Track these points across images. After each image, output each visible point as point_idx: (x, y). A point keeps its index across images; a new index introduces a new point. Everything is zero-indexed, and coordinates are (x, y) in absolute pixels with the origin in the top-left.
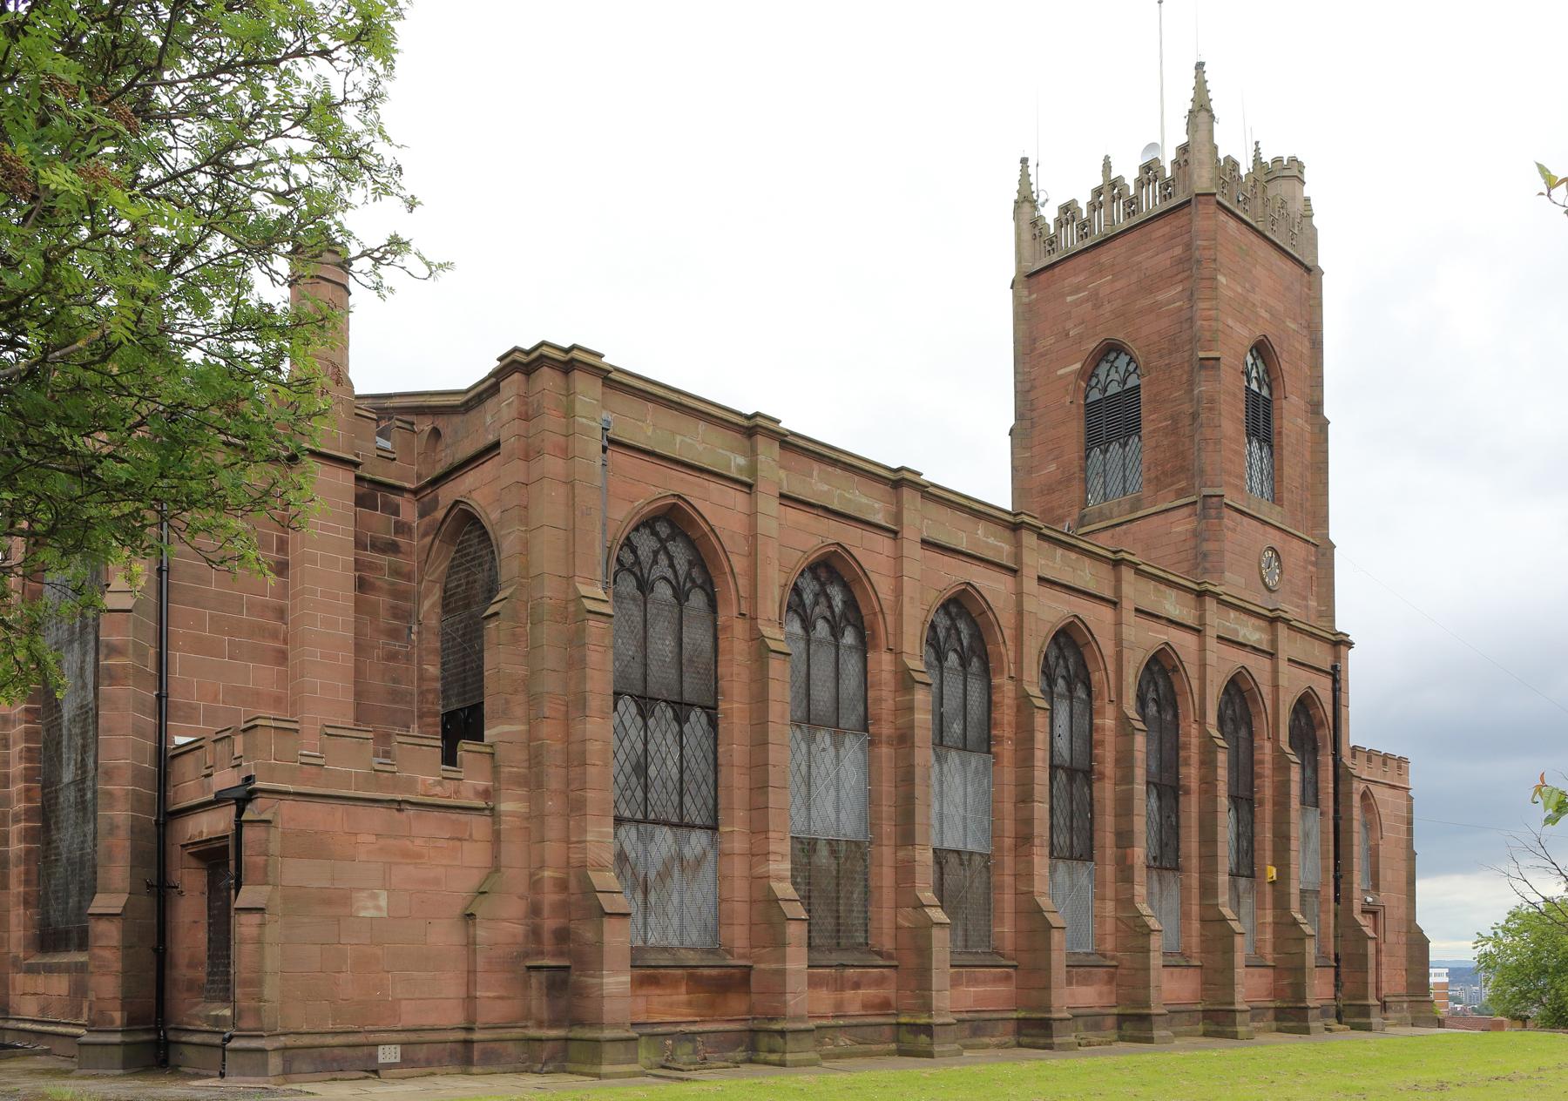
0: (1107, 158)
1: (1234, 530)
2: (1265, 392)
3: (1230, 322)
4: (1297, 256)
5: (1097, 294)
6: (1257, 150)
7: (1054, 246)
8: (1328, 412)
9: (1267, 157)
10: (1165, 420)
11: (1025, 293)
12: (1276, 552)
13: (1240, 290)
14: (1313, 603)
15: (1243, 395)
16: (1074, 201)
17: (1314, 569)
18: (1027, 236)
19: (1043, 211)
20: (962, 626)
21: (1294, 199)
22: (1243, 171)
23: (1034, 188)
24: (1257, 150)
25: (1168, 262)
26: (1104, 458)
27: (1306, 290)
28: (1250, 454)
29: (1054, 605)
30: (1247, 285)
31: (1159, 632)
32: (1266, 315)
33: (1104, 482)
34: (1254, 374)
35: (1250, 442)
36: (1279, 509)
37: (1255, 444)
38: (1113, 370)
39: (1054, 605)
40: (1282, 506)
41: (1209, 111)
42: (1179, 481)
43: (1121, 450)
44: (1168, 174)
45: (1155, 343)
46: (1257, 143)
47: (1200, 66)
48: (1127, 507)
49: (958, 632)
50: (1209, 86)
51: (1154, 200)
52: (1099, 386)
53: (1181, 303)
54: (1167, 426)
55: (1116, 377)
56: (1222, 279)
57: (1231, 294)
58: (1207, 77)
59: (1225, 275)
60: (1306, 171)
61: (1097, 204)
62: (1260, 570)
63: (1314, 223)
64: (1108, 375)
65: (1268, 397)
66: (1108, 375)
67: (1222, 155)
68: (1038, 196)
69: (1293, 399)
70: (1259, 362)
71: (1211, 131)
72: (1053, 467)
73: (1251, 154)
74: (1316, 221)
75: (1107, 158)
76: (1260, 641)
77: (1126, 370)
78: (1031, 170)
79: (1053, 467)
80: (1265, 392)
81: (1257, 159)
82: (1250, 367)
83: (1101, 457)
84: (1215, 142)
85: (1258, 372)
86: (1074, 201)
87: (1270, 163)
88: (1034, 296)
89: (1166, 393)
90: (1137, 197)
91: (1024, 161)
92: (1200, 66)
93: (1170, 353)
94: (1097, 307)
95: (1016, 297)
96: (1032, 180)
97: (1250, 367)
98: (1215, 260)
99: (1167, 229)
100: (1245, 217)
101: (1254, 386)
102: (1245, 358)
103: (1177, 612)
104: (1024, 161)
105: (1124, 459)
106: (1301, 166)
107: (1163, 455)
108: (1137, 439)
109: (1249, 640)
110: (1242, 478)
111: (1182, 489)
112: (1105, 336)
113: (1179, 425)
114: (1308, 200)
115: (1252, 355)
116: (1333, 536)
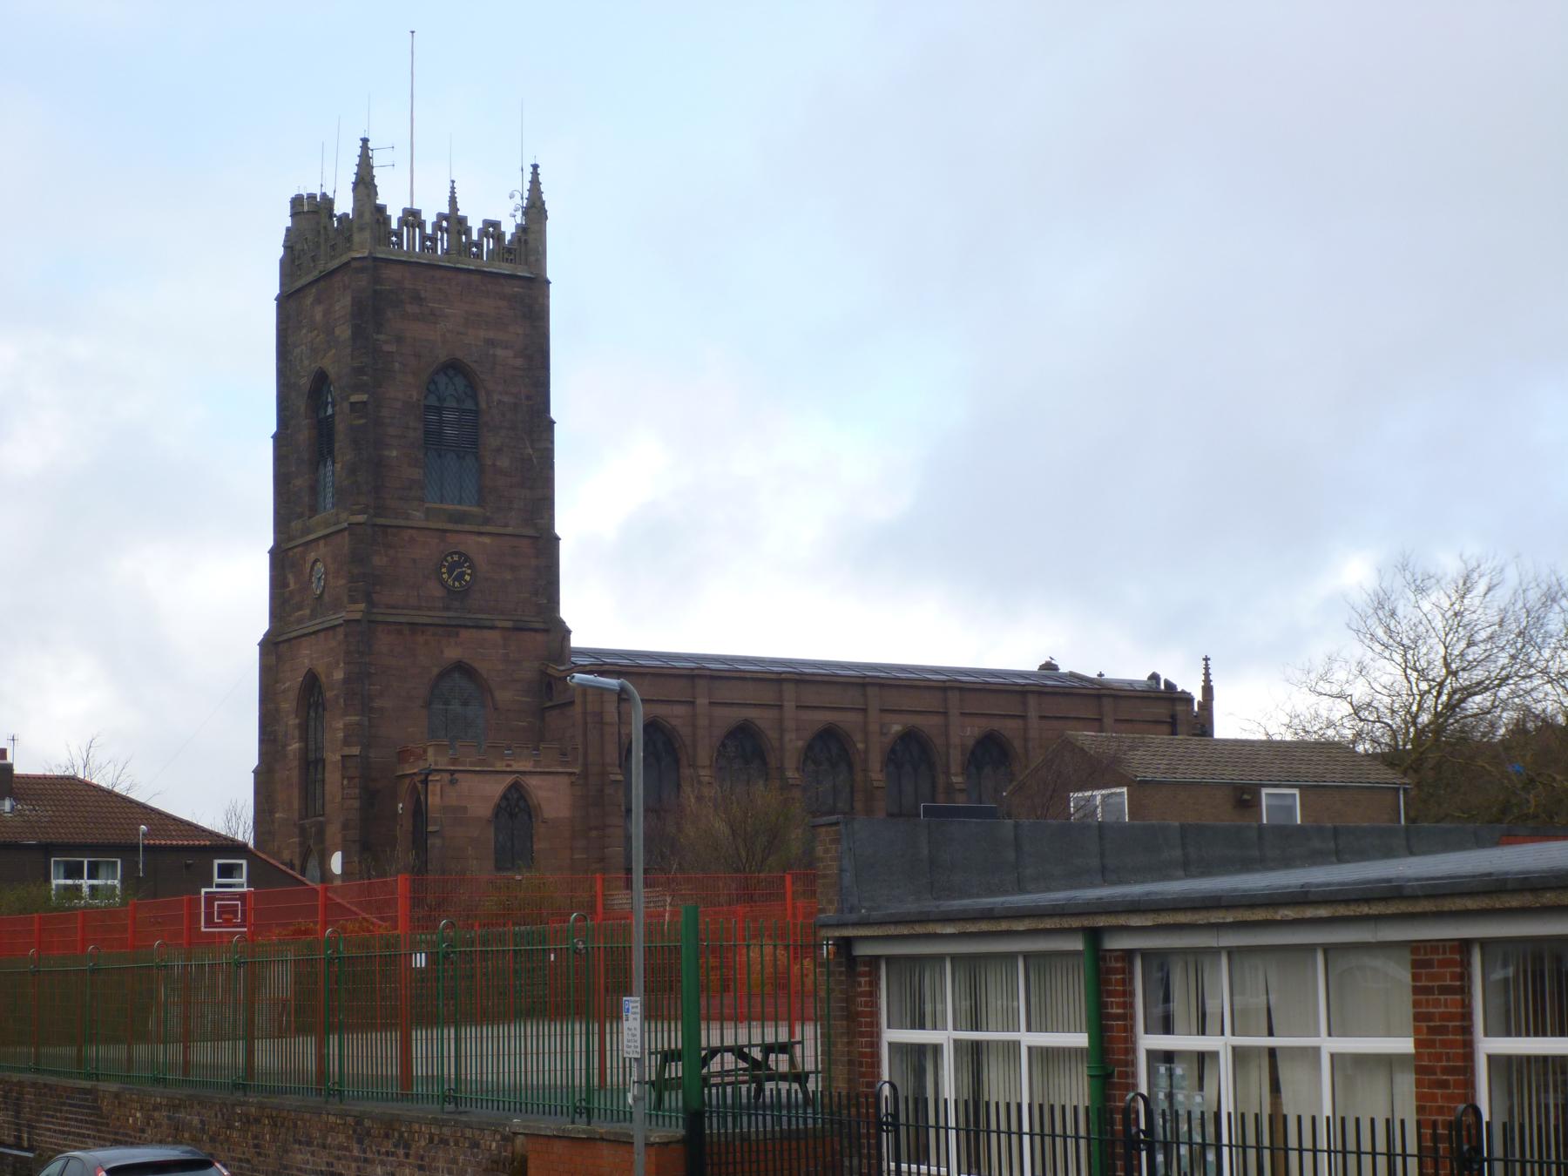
6: (453, 188)
9: (393, 200)
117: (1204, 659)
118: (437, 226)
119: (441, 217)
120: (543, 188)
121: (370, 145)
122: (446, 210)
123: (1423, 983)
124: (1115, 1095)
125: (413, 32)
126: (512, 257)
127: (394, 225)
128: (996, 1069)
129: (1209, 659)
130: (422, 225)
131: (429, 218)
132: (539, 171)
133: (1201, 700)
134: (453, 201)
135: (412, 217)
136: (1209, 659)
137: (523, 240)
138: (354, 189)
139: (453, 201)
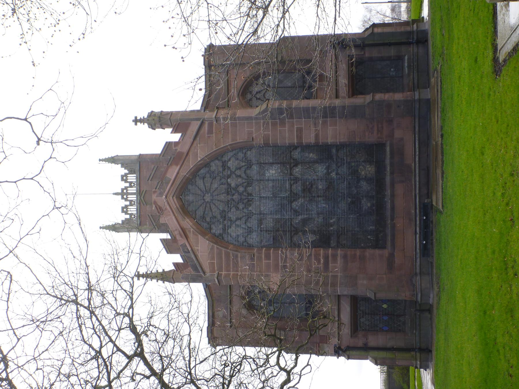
117: (136, 124)
118: (126, 200)
119: (123, 198)
120: (107, 157)
121: (102, 226)
122: (120, 196)
123: (313, 97)
124: (285, 127)
125: (165, 46)
126: (133, 169)
127: (128, 216)
128: (390, 344)
129: (136, 117)
130: (126, 188)
131: (125, 203)
132: (101, 159)
133: (170, 130)
134: (142, 121)
135: (124, 209)
136: (136, 117)
137: (126, 166)
138: (118, 232)
139: (142, 121)
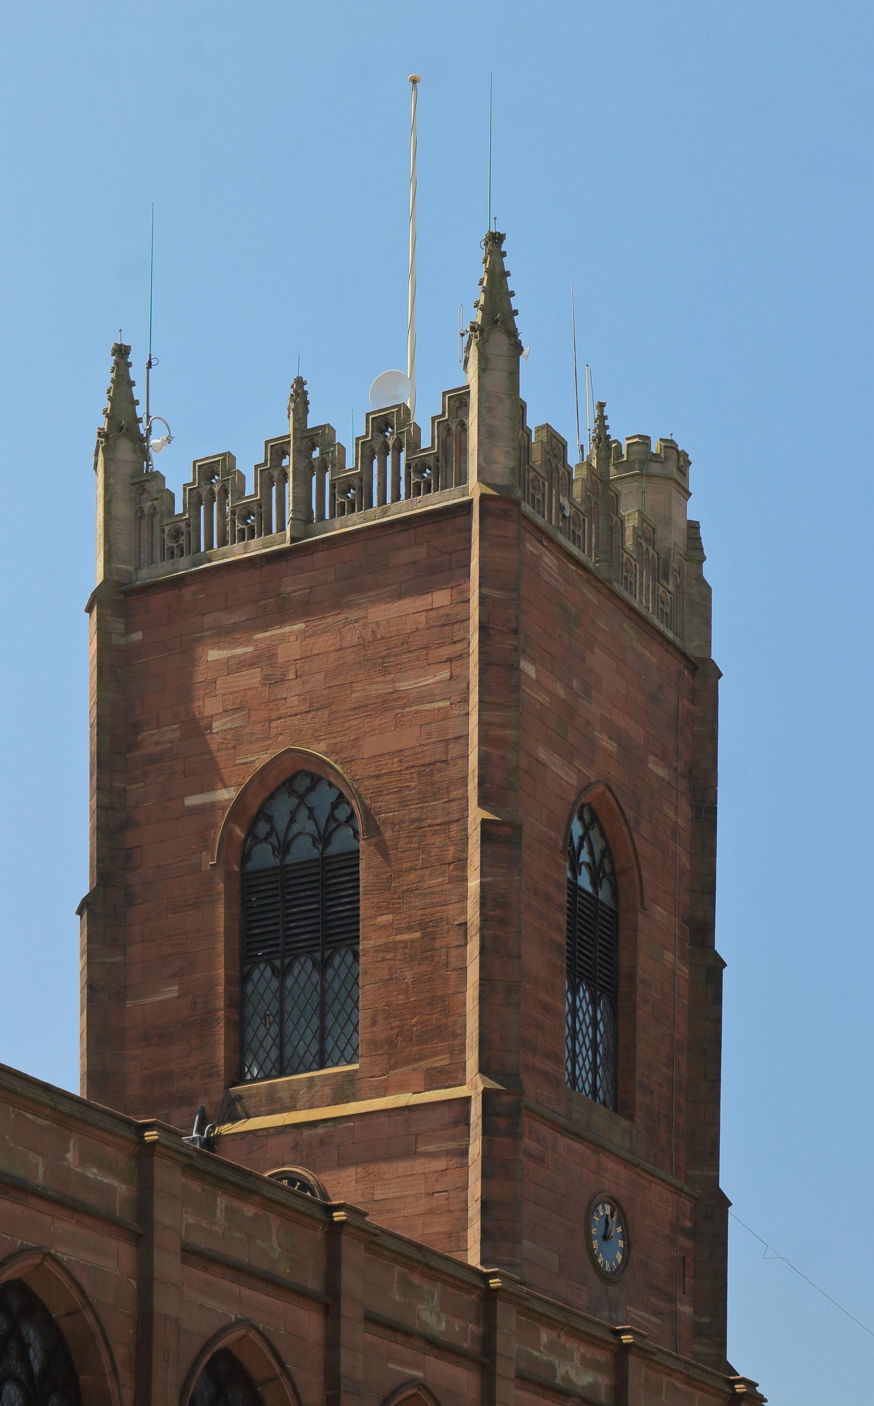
0: (300, 382)
1: (540, 1160)
2: (604, 895)
3: (542, 753)
4: (670, 635)
5: (274, 655)
6: (602, 418)
7: (183, 540)
8: (722, 946)
10: (410, 929)
11: (119, 626)
12: (620, 1207)
13: (561, 693)
14: (686, 1309)
15: (562, 898)
16: (228, 459)
17: (687, 1243)
18: (123, 510)
19: (159, 462)
20: (30, 1333)
21: (668, 521)
22: (573, 459)
23: (140, 411)
24: (602, 418)
25: (422, 618)
26: (282, 986)
27: (686, 703)
28: (574, 1011)
29: (210, 1303)
30: (575, 683)
31: (409, 1365)
32: (610, 746)
33: (281, 1034)
34: (584, 857)
35: (575, 991)
36: (624, 1123)
37: (584, 993)
38: (303, 813)
39: (210, 1303)
40: (631, 1118)
41: (512, 334)
42: (435, 1054)
43: (316, 977)
44: (426, 442)
45: (390, 773)
46: (601, 406)
47: (495, 240)
48: (327, 1090)
49: (24, 1347)
50: (512, 283)
51: (590, 944)
52: (273, 840)
53: (446, 703)
54: (413, 941)
55: (310, 826)
56: (529, 668)
57: (544, 699)
58: (508, 264)
59: (533, 661)
60: (692, 471)
61: (276, 473)
62: (590, 1250)
63: (706, 575)
64: (292, 820)
65: (610, 903)
66: (292, 820)
67: (533, 422)
68: (149, 431)
69: (659, 912)
70: (594, 834)
71: (514, 375)
72: (172, 992)
73: (589, 423)
74: (709, 571)
75: (300, 382)
76: (594, 1386)
77: (332, 817)
78: (136, 373)
79: (172, 992)
80: (604, 895)
81: (602, 439)
82: (576, 842)
83: (275, 984)
84: (522, 396)
85: (591, 853)
86: (228, 459)
87: (624, 444)
88: (138, 636)
89: (413, 876)
90: (360, 476)
91: (121, 352)
92: (495, 240)
93: (423, 798)
94: (274, 681)
95: (103, 633)
96: (138, 392)
97: (576, 842)
98: (515, 631)
99: (421, 552)
100: (574, 549)
101: (584, 880)
102: (569, 825)
103: (443, 1326)
104: (121, 352)
105: (324, 992)
106: (682, 462)
107: (402, 998)
108: (349, 958)
109: (574, 1384)
110: (556, 1058)
111: (441, 1071)
112: (284, 744)
113: (437, 944)
114: (694, 527)
115: (581, 819)
116: (727, 1184)
